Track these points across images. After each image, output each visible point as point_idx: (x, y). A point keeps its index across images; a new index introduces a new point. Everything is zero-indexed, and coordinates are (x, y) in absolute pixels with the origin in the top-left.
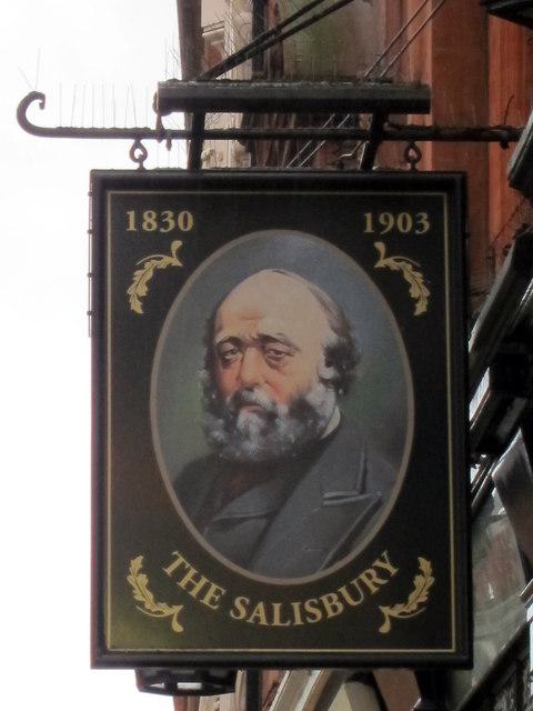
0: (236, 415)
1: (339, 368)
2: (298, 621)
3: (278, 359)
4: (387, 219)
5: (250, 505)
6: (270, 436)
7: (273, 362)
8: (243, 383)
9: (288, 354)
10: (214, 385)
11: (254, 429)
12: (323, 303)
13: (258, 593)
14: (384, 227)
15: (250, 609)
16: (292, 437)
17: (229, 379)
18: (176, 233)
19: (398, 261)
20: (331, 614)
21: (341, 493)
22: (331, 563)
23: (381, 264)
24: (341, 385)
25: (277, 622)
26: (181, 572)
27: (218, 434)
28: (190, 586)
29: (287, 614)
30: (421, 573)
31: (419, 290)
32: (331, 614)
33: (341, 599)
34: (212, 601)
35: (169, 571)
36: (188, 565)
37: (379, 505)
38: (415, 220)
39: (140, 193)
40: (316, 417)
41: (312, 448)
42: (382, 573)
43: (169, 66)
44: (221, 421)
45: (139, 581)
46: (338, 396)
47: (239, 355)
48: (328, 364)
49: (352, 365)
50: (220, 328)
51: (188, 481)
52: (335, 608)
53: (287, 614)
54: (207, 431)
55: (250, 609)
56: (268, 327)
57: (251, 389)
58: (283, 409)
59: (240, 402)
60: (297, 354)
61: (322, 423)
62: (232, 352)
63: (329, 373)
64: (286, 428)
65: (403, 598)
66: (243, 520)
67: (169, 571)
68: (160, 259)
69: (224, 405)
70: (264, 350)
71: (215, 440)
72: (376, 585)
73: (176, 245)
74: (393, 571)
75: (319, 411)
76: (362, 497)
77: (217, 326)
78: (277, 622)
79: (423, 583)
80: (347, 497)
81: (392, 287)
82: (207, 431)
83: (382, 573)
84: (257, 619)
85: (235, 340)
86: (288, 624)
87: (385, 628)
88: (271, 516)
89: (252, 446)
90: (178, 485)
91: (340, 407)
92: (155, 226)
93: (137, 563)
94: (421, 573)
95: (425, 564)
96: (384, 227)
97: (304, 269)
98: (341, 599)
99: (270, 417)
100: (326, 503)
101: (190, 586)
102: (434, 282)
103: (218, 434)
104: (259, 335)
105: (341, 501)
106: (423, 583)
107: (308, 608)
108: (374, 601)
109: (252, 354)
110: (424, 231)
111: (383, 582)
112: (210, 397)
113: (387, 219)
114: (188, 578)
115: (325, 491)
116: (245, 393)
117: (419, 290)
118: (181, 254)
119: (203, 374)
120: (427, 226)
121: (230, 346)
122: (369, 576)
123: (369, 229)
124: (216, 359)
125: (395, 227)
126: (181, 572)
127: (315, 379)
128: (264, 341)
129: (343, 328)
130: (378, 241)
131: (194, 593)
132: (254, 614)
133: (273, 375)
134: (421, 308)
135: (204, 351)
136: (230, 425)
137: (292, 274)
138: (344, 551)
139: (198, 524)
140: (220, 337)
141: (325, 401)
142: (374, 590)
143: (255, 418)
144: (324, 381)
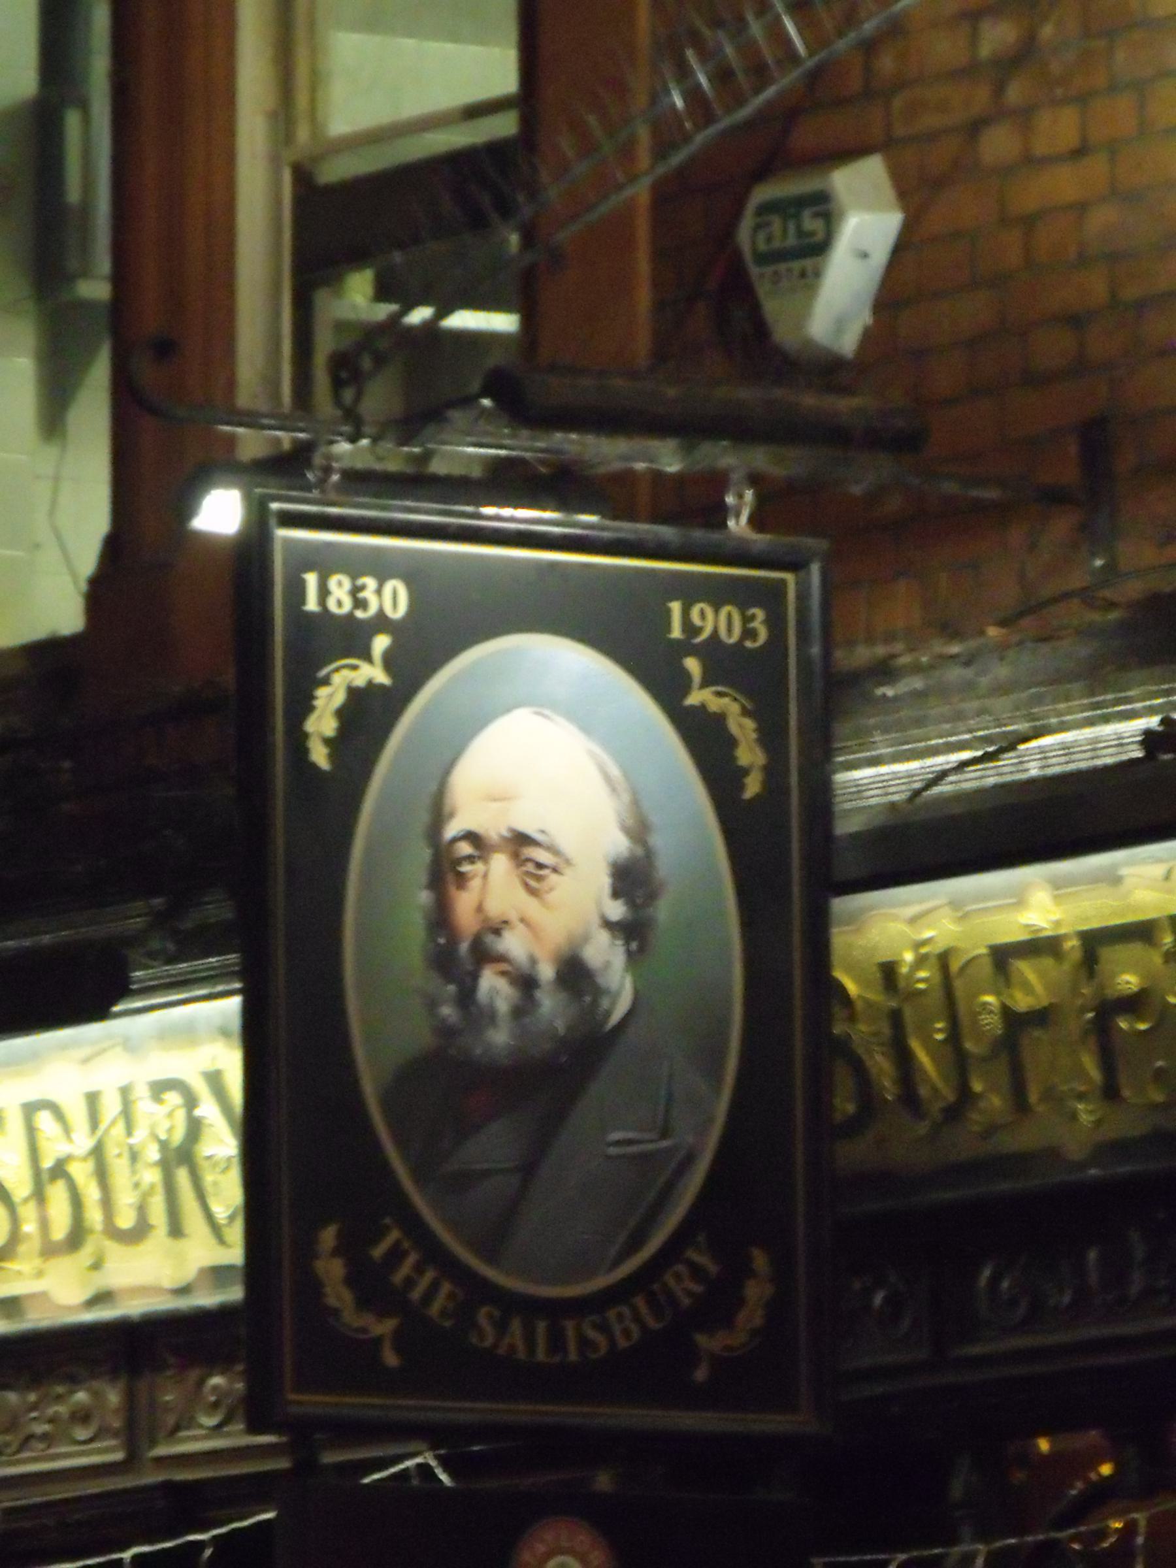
0: (475, 976)
1: (632, 904)
2: (573, 1356)
3: (539, 878)
4: (703, 614)
6: (527, 1020)
7: (533, 883)
8: (486, 920)
9: (555, 870)
11: (503, 1006)
12: (608, 779)
14: (698, 631)
15: (501, 1327)
16: (560, 1026)
17: (464, 904)
18: (381, 623)
19: (719, 694)
20: (622, 1343)
21: (631, 1135)
22: (616, 1263)
23: (695, 698)
25: (541, 1355)
26: (395, 1255)
27: (447, 1011)
28: (409, 1283)
29: (557, 1342)
30: (327, 742)
31: (750, 755)
32: (622, 1343)
33: (637, 1318)
34: (443, 1313)
35: (378, 1252)
36: (406, 1245)
37: (689, 1159)
38: (747, 620)
40: (598, 991)
42: (696, 1271)
44: (451, 988)
46: (630, 954)
47: (479, 867)
48: (616, 894)
49: (652, 896)
50: (452, 815)
52: (627, 1333)
53: (557, 1342)
54: (432, 1004)
55: (501, 1327)
57: (497, 932)
58: (547, 972)
59: (483, 954)
60: (568, 871)
61: (605, 1003)
62: (471, 859)
63: (617, 910)
65: (727, 1322)
66: (486, 1174)
67: (378, 1252)
68: (354, 668)
70: (518, 860)
71: (443, 1020)
72: (690, 1294)
73: (381, 643)
74: (713, 1268)
75: (601, 981)
76: (665, 1144)
77: (447, 809)
78: (541, 1355)
79: (756, 1292)
80: (639, 1142)
82: (432, 1004)
83: (696, 1271)
84: (512, 1348)
85: (472, 837)
86: (557, 1359)
87: (701, 1374)
88: (528, 1170)
89: (500, 1037)
90: (388, 1102)
91: (634, 975)
92: (348, 605)
93: (328, 1236)
94: (327, 742)
95: (760, 1260)
96: (698, 631)
98: (637, 1318)
99: (526, 983)
100: (613, 1151)
101: (409, 1283)
103: (447, 1011)
104: (512, 830)
105: (633, 1149)
106: (756, 1292)
107: (592, 1334)
109: (500, 863)
110: (757, 644)
111: (698, 1288)
112: (435, 941)
113: (703, 614)
114: (405, 1269)
116: (489, 939)
117: (750, 755)
118: (390, 661)
119: (425, 897)
120: (763, 635)
121: (465, 848)
122: (678, 1277)
123: (676, 633)
125: (715, 631)
126: (395, 1255)
127: (596, 921)
128: (520, 841)
129: (639, 830)
130: (689, 654)
131: (416, 1294)
132: (507, 1340)
133: (531, 906)
134: (753, 786)
135: (426, 854)
136: (467, 996)
137: (561, 720)
138: (636, 1242)
139: (421, 1175)
140: (452, 830)
142: (686, 1301)
143: (503, 985)
144: (608, 924)
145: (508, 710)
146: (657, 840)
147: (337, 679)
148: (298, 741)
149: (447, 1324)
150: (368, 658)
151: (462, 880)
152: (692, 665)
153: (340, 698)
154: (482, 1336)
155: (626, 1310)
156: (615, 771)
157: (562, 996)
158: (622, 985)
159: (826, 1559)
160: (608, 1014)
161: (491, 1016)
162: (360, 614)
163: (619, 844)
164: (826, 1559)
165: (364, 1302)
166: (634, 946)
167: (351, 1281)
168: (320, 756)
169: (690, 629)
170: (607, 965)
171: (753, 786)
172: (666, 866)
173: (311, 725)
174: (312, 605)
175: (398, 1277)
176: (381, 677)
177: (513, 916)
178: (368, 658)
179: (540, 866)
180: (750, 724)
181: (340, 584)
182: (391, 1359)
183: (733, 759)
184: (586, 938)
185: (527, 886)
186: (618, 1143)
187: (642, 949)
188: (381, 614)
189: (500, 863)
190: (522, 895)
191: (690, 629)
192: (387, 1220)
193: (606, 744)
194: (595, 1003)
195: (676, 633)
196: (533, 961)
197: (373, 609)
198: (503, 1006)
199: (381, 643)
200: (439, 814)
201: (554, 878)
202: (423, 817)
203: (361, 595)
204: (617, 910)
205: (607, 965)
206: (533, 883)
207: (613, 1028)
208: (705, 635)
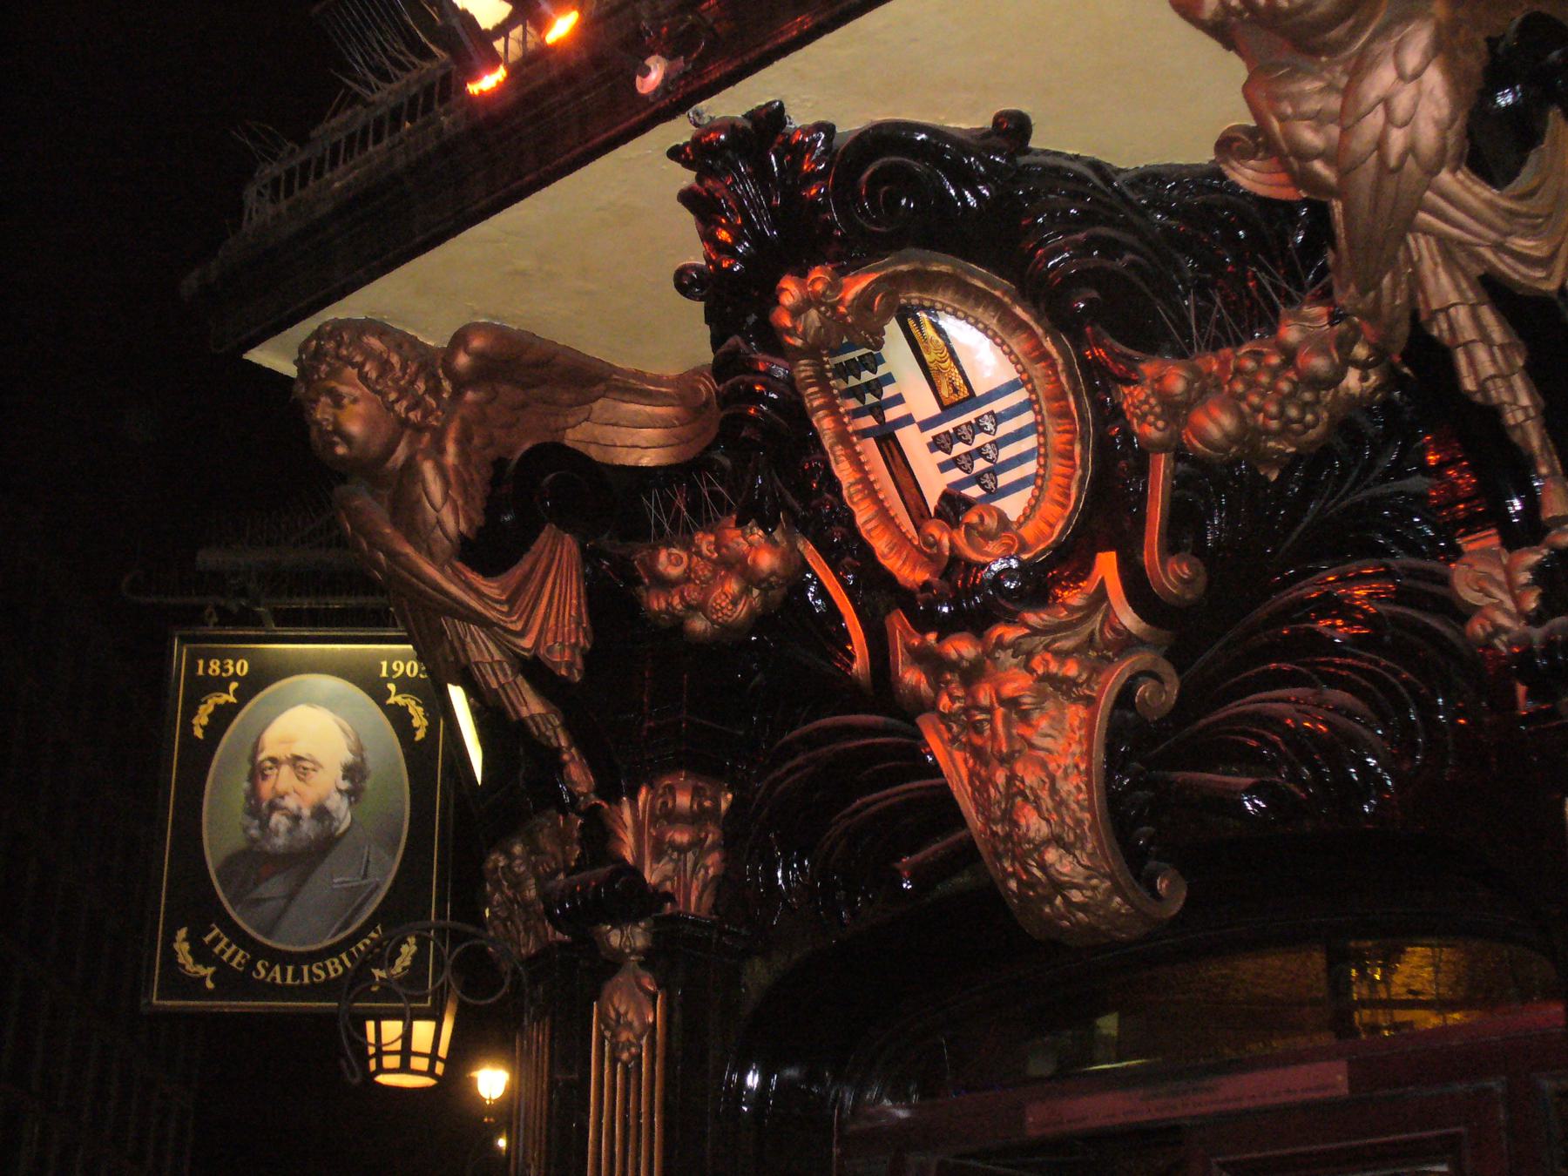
0: (269, 818)
1: (352, 780)
2: (306, 980)
4: (398, 666)
7: (302, 776)
8: (277, 792)
9: (314, 770)
11: (282, 829)
12: (344, 730)
13: (282, 958)
14: (396, 672)
17: (266, 788)
18: (235, 677)
20: (333, 975)
22: (334, 935)
23: (391, 701)
25: (289, 980)
26: (216, 941)
27: (254, 832)
28: (223, 952)
29: (298, 974)
34: (239, 964)
35: (207, 939)
36: (222, 935)
37: (377, 887)
40: (332, 819)
44: (257, 822)
46: (350, 803)
48: (344, 778)
49: (364, 778)
50: (262, 751)
51: (231, 865)
52: (336, 971)
53: (298, 974)
54: (246, 829)
58: (306, 812)
59: (273, 807)
60: (320, 771)
61: (336, 824)
63: (345, 785)
67: (207, 939)
70: (294, 766)
73: (234, 686)
76: (364, 882)
77: (260, 749)
82: (246, 829)
85: (273, 760)
86: (298, 982)
88: (291, 897)
89: (280, 841)
92: (218, 671)
99: (296, 818)
100: (335, 886)
101: (223, 952)
102: (170, 955)
103: (254, 832)
109: (285, 770)
113: (398, 666)
114: (222, 945)
115: (333, 878)
116: (278, 801)
118: (237, 693)
119: (246, 785)
121: (269, 764)
123: (384, 674)
125: (405, 672)
126: (216, 941)
128: (296, 760)
129: (358, 750)
131: (225, 957)
132: (272, 974)
135: (249, 767)
136: (264, 825)
140: (262, 757)
141: (339, 806)
144: (340, 791)
145: (294, 705)
146: (366, 755)
147: (210, 701)
148: (188, 727)
149: (241, 969)
150: (228, 693)
151: (265, 777)
152: (392, 687)
153: (211, 709)
154: (258, 973)
155: (336, 961)
156: (348, 728)
157: (315, 823)
158: (345, 816)
159: (386, 132)
160: (337, 829)
161: (276, 833)
162: (224, 675)
163: (347, 757)
164: (386, 132)
165: (197, 961)
166: (353, 799)
167: (191, 952)
168: (199, 733)
169: (390, 671)
170: (339, 808)
171: (420, 735)
172: (372, 762)
173: (195, 721)
174: (200, 672)
175: (217, 950)
176: (232, 699)
177: (290, 790)
178: (228, 693)
179: (305, 769)
180: (420, 709)
181: (215, 663)
182: (210, 985)
183: (411, 723)
184: (328, 797)
185: (299, 778)
186: (339, 883)
187: (356, 801)
188: (235, 673)
189: (285, 770)
190: (296, 782)
191: (390, 671)
192: (213, 925)
193: (346, 718)
194: (331, 825)
195: (384, 674)
196: (300, 808)
197: (231, 670)
198: (282, 829)
199: (234, 686)
200: (256, 748)
201: (313, 773)
202: (248, 751)
203: (226, 667)
204: (345, 785)
205: (339, 808)
206: (302, 776)
207: (1540, 392)
208: (398, 675)
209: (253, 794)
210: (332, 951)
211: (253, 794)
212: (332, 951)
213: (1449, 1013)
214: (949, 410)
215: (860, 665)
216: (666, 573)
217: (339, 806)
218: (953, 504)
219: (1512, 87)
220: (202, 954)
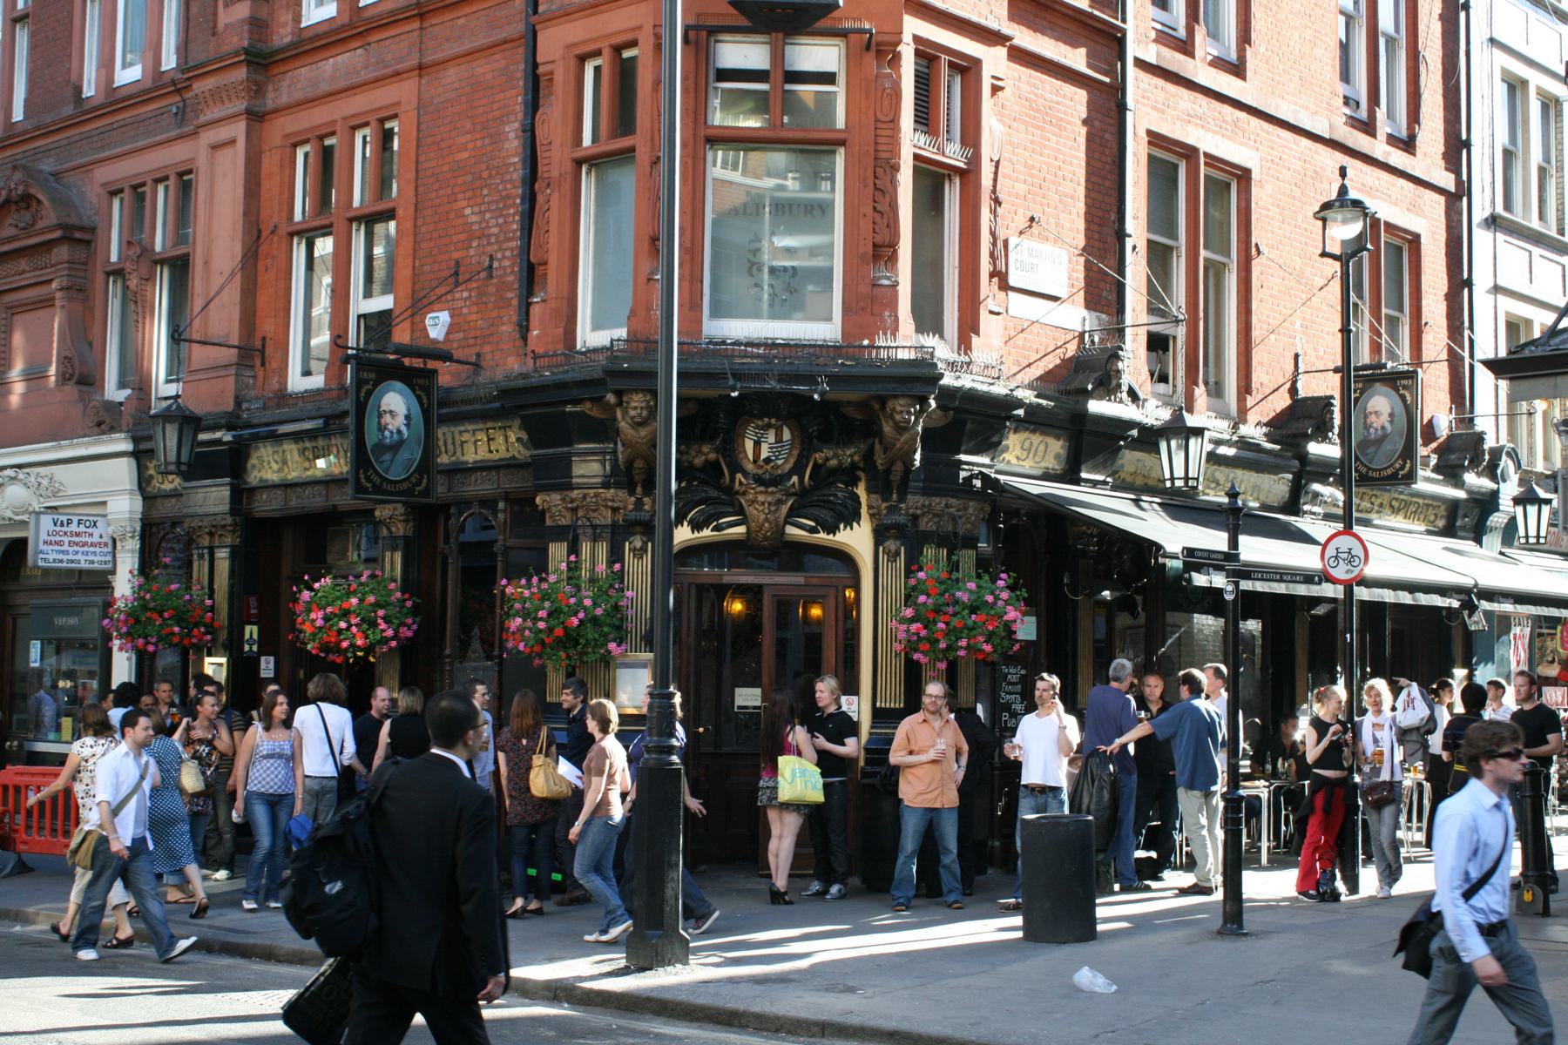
5: (387, 457)
10: (379, 423)
13: (1374, 470)
24: (408, 425)
39: (55, 352)
41: (401, 442)
43: (1492, 284)
45: (362, 476)
51: (375, 447)
56: (392, 408)
59: (386, 428)
64: (1380, 432)
69: (1367, 427)
79: (425, 481)
81: (1403, 398)
89: (1373, 437)
97: (400, 393)
99: (392, 433)
108: (1398, 470)
115: (404, 454)
117: (425, 401)
124: (380, 416)
128: (391, 412)
129: (409, 410)
141: (1387, 425)
209: (1365, 423)
210: (1388, 467)
211: (1365, 423)
212: (1388, 467)
213: (26, 566)
214: (776, 442)
215: (1465, 276)
216: (520, 150)
217: (1387, 425)
218: (768, 460)
219: (785, 749)
220: (368, 479)
